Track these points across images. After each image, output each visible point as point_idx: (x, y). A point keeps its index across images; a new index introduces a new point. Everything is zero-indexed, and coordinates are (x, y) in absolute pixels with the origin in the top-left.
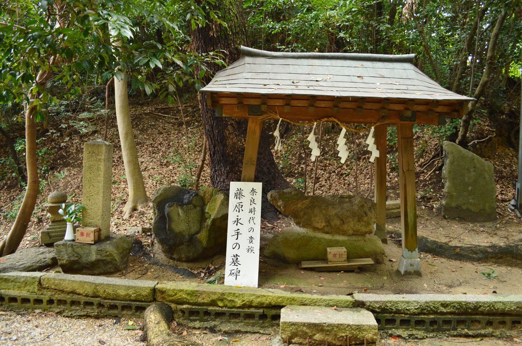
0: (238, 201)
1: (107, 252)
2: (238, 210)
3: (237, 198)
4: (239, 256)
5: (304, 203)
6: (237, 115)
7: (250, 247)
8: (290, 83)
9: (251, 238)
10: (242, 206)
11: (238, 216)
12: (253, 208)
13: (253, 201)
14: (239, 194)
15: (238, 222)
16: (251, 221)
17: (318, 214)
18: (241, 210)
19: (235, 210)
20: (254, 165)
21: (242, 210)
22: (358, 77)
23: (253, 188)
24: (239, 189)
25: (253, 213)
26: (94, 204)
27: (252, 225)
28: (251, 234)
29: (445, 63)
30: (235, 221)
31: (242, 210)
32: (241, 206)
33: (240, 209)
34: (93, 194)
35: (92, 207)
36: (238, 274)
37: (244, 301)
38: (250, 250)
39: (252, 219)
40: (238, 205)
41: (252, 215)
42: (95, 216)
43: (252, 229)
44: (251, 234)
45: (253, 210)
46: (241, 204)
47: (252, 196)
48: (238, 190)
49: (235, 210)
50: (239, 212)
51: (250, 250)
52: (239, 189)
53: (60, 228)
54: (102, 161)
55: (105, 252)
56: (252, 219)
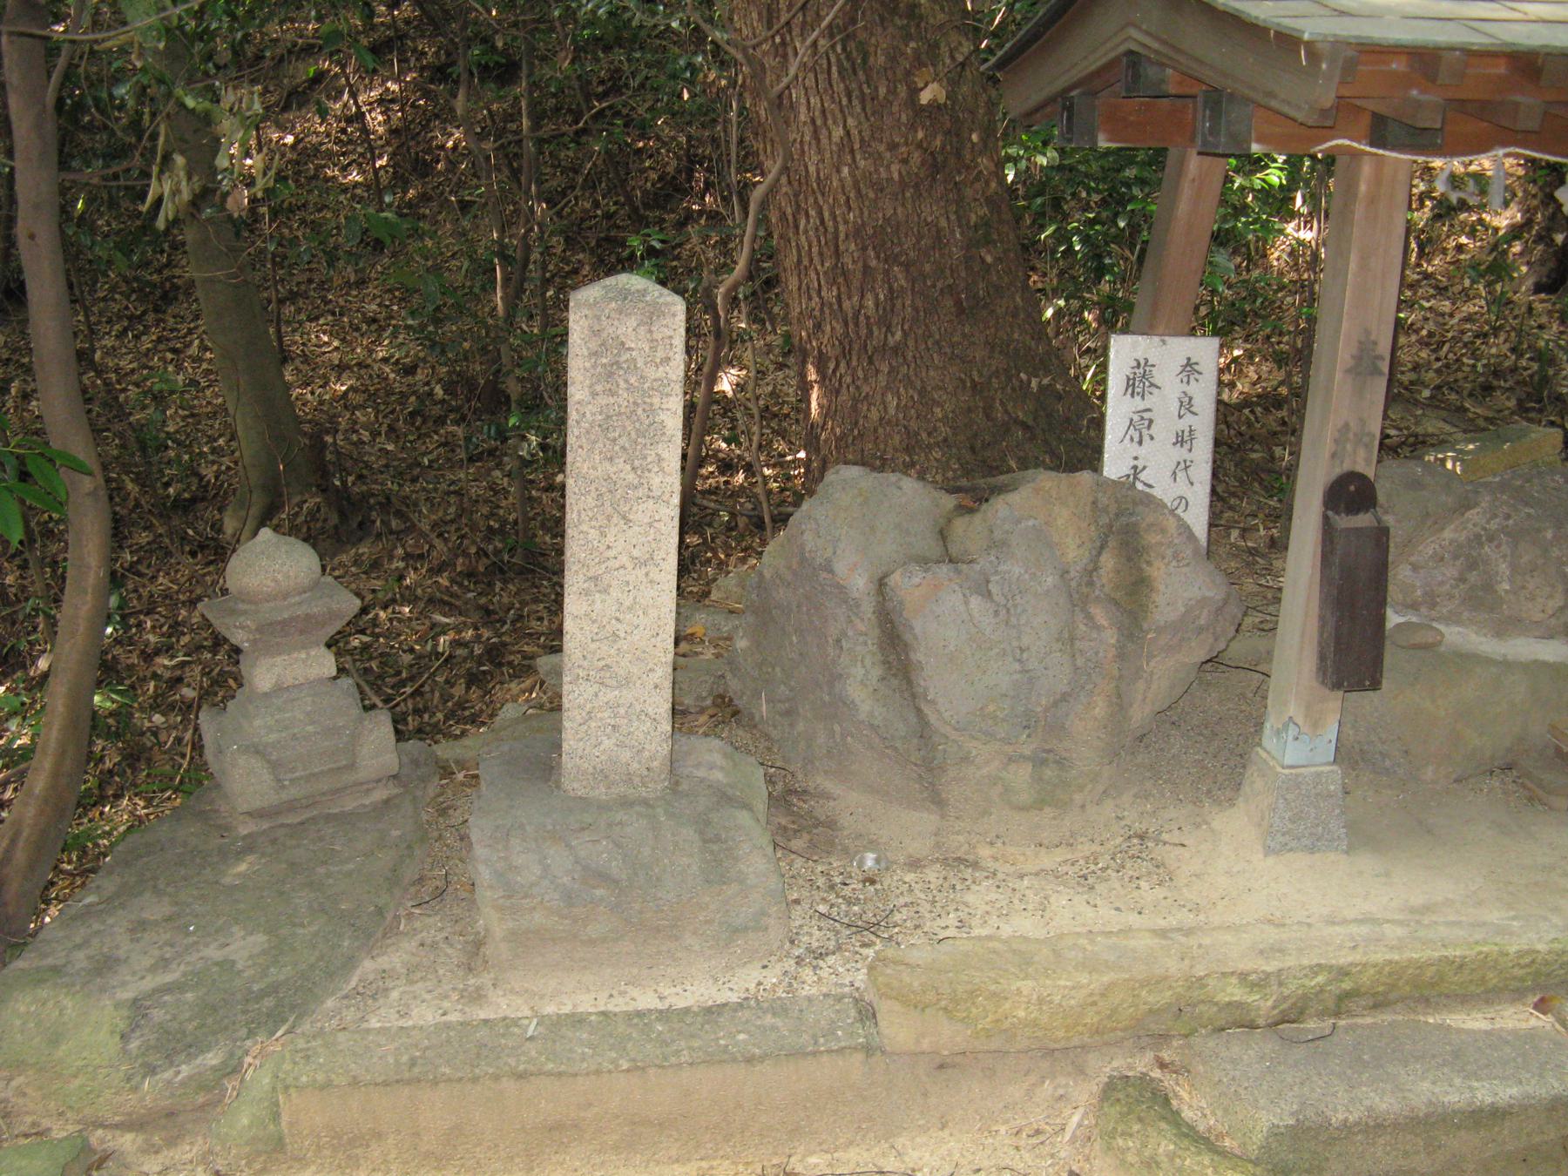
3: (1132, 395)
10: (1151, 421)
11: (1136, 458)
14: (1140, 381)
16: (1181, 475)
18: (1146, 438)
19: (1128, 437)
21: (1152, 438)
23: (1189, 359)
24: (1142, 363)
25: (1187, 446)
26: (630, 608)
31: (1152, 438)
32: (1146, 423)
33: (1145, 432)
40: (1136, 418)
45: (1186, 434)
46: (1146, 415)
47: (1185, 387)
49: (1128, 437)
50: (1140, 443)
52: (1142, 363)
56: (1182, 465)
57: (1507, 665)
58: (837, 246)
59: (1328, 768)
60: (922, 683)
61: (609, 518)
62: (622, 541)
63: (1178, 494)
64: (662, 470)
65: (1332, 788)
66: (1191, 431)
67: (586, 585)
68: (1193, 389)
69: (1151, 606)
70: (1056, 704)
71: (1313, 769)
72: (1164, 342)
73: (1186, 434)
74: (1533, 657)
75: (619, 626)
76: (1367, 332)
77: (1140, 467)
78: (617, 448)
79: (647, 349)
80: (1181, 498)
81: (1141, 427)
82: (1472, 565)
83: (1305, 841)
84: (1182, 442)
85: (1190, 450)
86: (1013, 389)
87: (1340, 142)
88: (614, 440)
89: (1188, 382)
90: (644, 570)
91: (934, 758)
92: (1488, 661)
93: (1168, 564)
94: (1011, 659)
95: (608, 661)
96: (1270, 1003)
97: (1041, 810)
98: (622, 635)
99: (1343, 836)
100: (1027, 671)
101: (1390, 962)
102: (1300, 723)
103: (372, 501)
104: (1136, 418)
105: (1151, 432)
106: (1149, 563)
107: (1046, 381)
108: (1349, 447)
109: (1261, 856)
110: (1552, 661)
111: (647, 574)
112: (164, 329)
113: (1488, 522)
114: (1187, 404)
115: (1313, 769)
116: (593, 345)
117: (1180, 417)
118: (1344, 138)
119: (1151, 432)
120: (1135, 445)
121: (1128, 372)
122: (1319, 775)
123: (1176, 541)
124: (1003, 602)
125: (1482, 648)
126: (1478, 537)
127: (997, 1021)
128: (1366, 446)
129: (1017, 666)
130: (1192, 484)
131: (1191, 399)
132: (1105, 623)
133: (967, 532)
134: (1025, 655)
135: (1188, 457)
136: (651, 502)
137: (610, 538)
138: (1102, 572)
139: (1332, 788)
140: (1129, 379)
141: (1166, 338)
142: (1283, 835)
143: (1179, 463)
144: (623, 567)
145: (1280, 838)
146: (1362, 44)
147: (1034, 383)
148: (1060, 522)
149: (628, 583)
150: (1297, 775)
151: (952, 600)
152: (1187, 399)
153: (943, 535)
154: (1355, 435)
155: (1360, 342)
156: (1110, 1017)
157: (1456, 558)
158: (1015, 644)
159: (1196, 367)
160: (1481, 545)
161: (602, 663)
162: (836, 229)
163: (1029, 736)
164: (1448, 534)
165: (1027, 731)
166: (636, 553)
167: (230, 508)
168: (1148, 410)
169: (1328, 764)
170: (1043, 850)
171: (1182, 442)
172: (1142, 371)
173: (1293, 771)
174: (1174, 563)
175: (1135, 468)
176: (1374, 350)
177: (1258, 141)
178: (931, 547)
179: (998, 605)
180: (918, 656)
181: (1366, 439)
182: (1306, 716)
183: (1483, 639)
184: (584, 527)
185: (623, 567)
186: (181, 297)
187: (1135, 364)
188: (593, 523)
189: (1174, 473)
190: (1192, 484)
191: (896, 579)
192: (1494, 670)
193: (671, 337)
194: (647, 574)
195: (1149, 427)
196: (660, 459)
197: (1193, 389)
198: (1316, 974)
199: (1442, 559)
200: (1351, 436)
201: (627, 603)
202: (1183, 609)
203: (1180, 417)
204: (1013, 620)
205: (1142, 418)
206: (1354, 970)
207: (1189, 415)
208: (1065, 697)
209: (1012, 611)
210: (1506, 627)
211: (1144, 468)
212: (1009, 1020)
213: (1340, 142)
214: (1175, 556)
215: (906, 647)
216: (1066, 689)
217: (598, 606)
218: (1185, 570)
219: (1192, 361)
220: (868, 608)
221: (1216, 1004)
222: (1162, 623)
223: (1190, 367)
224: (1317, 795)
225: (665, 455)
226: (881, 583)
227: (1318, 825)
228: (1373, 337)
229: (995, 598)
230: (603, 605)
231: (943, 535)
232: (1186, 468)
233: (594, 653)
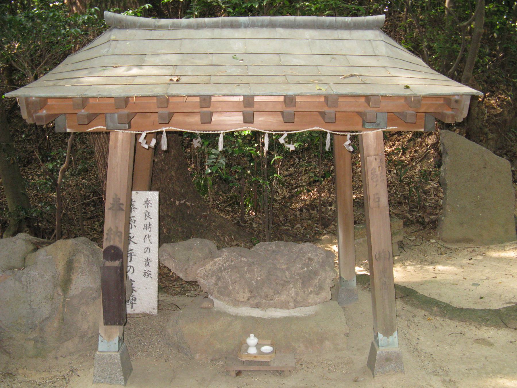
4: (134, 281)
5: (216, 262)
6: (43, 62)
7: (147, 271)
8: (183, 79)
9: (148, 260)
10: (135, 221)
12: (148, 224)
13: (147, 215)
16: (147, 240)
17: (238, 279)
20: (122, 210)
22: (355, 76)
23: (147, 199)
27: (147, 244)
28: (147, 255)
29: (54, 174)
31: (136, 227)
36: (133, 302)
38: (147, 274)
39: (147, 237)
41: (147, 232)
43: (148, 249)
44: (147, 255)
45: (148, 225)
47: (146, 209)
51: (147, 274)
56: (147, 237)
57: (236, 317)
58: (104, 156)
63: (146, 247)
65: (116, 361)
66: (150, 224)
69: (70, 289)
70: (43, 321)
71: (109, 353)
73: (148, 225)
74: (248, 315)
80: (147, 248)
82: (219, 279)
83: (107, 380)
85: (150, 231)
86: (167, 205)
87: (99, 127)
89: (148, 207)
92: (230, 315)
93: (78, 274)
97: (37, 358)
99: (122, 379)
100: (33, 309)
103: (47, 231)
105: (135, 224)
106: (73, 274)
107: (182, 202)
108: (112, 236)
109: (91, 383)
110: (256, 316)
112: (24, 172)
113: (225, 263)
115: (109, 353)
117: (145, 220)
118: (101, 126)
119: (135, 224)
122: (111, 356)
123: (83, 266)
124: (25, 284)
125: (229, 310)
126: (220, 268)
128: (119, 236)
129: (29, 307)
131: (149, 213)
134: (32, 303)
135: (148, 233)
139: (116, 361)
141: (138, 192)
142: (99, 376)
143: (146, 236)
145: (97, 378)
146: (41, 97)
147: (177, 203)
148: (59, 257)
150: (103, 355)
154: (114, 232)
155: (113, 199)
157: (212, 276)
158: (29, 299)
160: (221, 272)
162: (103, 150)
163: (32, 332)
164: (208, 267)
165: (31, 330)
167: (6, 231)
169: (116, 352)
170: (38, 373)
173: (101, 353)
174: (81, 274)
177: (69, 128)
179: (24, 285)
181: (119, 234)
183: (229, 307)
186: (33, 162)
189: (145, 239)
190: (151, 243)
192: (229, 319)
195: (134, 223)
199: (207, 276)
200: (113, 233)
202: (81, 291)
203: (145, 220)
204: (29, 291)
208: (46, 319)
209: (29, 288)
210: (237, 303)
211: (133, 237)
213: (99, 127)
214: (82, 272)
216: (48, 316)
218: (84, 277)
219: (149, 200)
222: (72, 295)
223: (147, 203)
224: (111, 363)
227: (112, 374)
228: (118, 197)
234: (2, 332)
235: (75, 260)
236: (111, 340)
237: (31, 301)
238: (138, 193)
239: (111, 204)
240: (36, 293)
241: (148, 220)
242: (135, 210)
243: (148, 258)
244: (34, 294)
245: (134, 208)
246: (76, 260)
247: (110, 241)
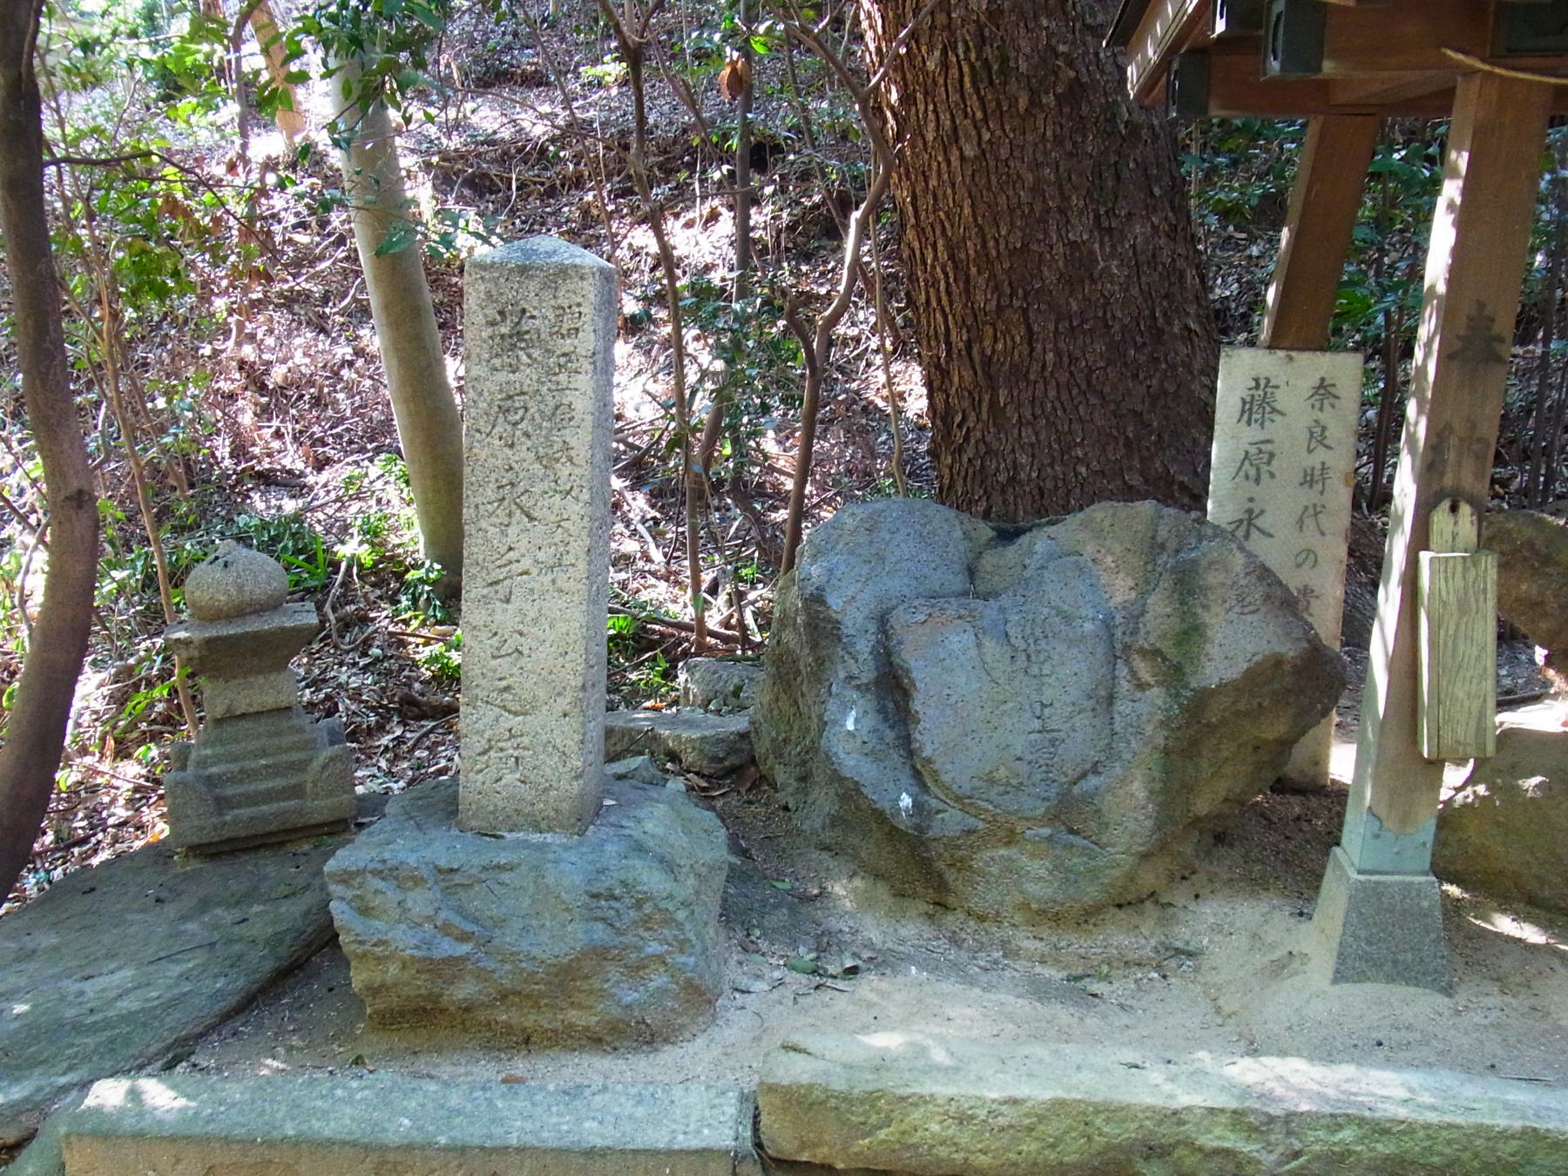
0: (1253, 433)
1: (639, 904)
2: (1252, 472)
3: (1249, 423)
10: (1272, 455)
11: (1251, 500)
14: (1258, 404)
15: (1250, 524)
16: (1309, 522)
18: (1265, 476)
19: (1242, 474)
21: (1272, 475)
24: (1263, 382)
25: (1319, 487)
26: (535, 621)
27: (1310, 538)
30: (1241, 521)
32: (1265, 457)
33: (1264, 468)
34: (526, 563)
35: (526, 644)
37: (1297, 1155)
40: (1253, 450)
42: (541, 694)
45: (1317, 473)
46: (1269, 447)
47: (1317, 414)
48: (1257, 387)
49: (1242, 474)
50: (1258, 481)
52: (1263, 382)
53: (264, 753)
54: (586, 365)
55: (628, 901)
56: (1311, 511)
59: (1424, 879)
60: (918, 737)
61: (510, 515)
62: (525, 541)
64: (570, 459)
65: (1425, 904)
67: (485, 591)
68: (1326, 417)
72: (1291, 359)
73: (1317, 473)
75: (523, 640)
76: (1481, 305)
77: (1257, 511)
78: (518, 433)
79: (552, 317)
80: (1309, 551)
81: (1257, 464)
84: (1311, 483)
85: (1322, 493)
88: (516, 424)
89: (1321, 409)
90: (550, 577)
91: (929, 827)
94: (1028, 715)
95: (510, 681)
96: (1273, 1157)
98: (526, 652)
101: (1450, 1126)
102: (1383, 816)
104: (1253, 450)
106: (1206, 607)
111: (554, 581)
114: (1318, 436)
116: (492, 312)
117: (1310, 451)
120: (1251, 483)
121: (1246, 394)
124: (1021, 644)
127: (904, 1133)
129: (1037, 724)
130: (1323, 534)
131: (1324, 429)
132: (1151, 680)
133: (996, 561)
134: (1047, 711)
136: (558, 496)
137: (512, 537)
138: (1148, 617)
139: (1425, 904)
140: (1244, 402)
141: (1294, 354)
143: (1306, 508)
144: (526, 573)
149: (532, 590)
151: (959, 640)
152: (1318, 430)
153: (972, 572)
155: (1471, 319)
156: (1053, 1146)
159: (1332, 390)
161: (504, 683)
166: (541, 556)
168: (1268, 441)
169: (1426, 874)
171: (1311, 483)
172: (1261, 392)
175: (1250, 511)
176: (1489, 329)
178: (958, 582)
179: (1016, 650)
180: (917, 705)
182: (1391, 806)
184: (484, 524)
185: (526, 573)
187: (1253, 384)
188: (494, 520)
190: (1323, 534)
191: (899, 618)
193: (579, 305)
194: (554, 581)
195: (1269, 463)
196: (566, 447)
197: (1326, 417)
198: (1340, 1127)
201: (532, 615)
203: (1310, 451)
204: (1035, 670)
205: (1261, 451)
206: (1395, 1130)
207: (1321, 449)
209: (1033, 658)
211: (1262, 512)
212: (919, 1134)
215: (906, 695)
217: (498, 616)
218: (1249, 618)
220: (864, 647)
221: (1200, 1149)
223: (1324, 390)
225: (573, 442)
226: (883, 621)
229: (1013, 640)
230: (505, 617)
231: (972, 572)
232: (1316, 514)
233: (495, 671)
234: (938, 812)
235: (1204, 563)
236: (1409, 830)
237: (1044, 706)
238: (1291, 359)
239: (1458, 337)
240: (1061, 676)
241: (1321, 455)
242: (1277, 418)
243: (1306, 587)
244: (1052, 680)
245: (1274, 410)
246: (1211, 564)
247: (1442, 474)
